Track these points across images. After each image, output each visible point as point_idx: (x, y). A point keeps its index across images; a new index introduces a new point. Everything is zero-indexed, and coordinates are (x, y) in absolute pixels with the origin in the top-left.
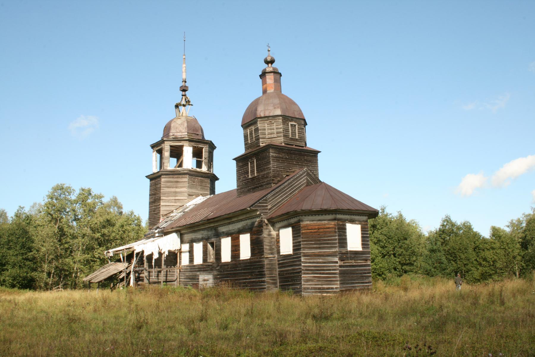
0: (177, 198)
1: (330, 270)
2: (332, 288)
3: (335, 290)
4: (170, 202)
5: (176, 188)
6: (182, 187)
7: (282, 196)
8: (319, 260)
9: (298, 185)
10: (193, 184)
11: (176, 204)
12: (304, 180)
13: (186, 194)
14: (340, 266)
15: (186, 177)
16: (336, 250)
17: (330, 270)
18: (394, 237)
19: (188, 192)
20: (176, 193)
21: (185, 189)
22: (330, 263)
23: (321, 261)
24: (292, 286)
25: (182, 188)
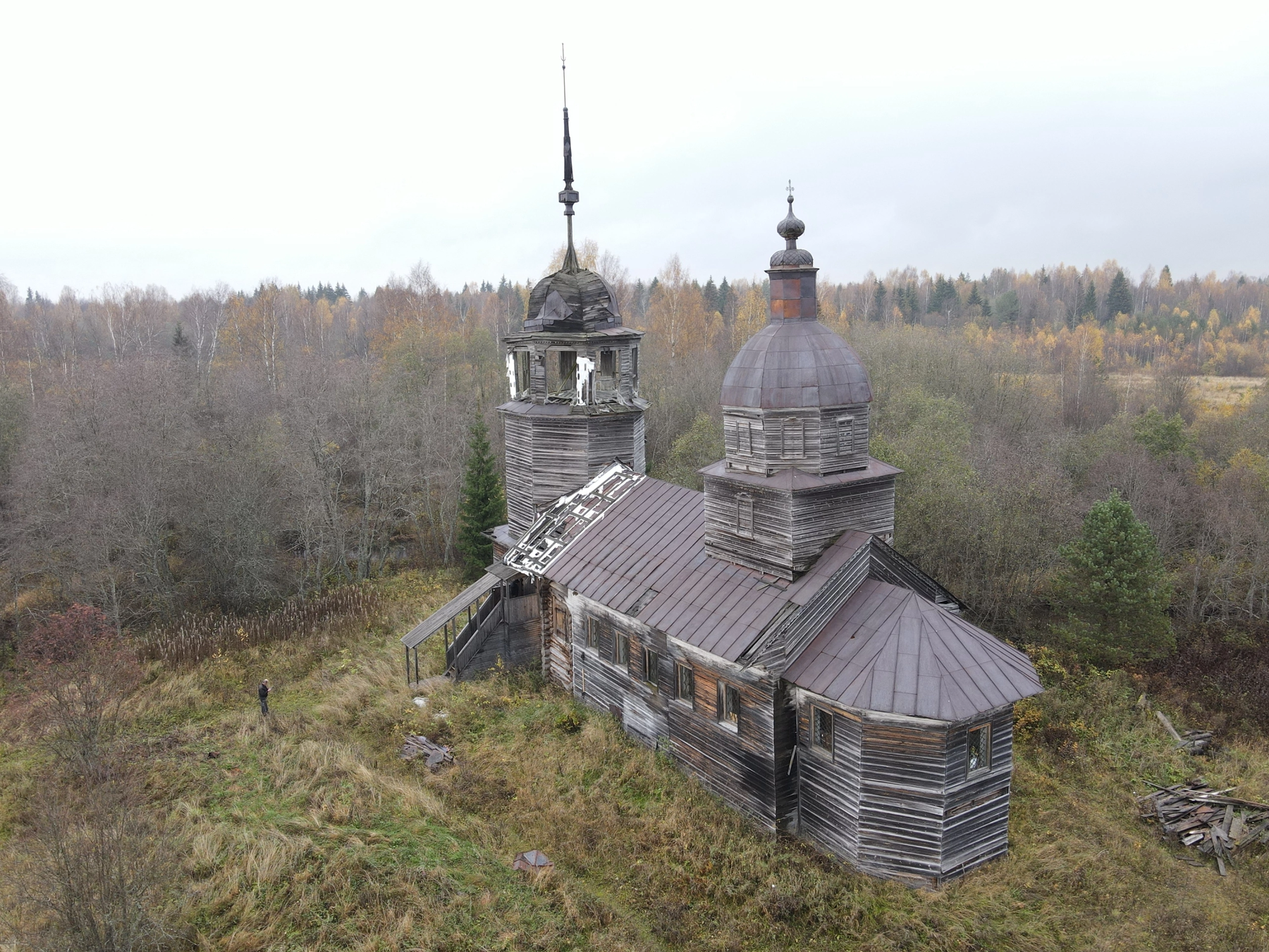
0: (566, 471)
1: (923, 829)
2: (925, 867)
3: (930, 871)
4: (552, 478)
5: (565, 449)
6: (577, 448)
7: (820, 612)
8: (898, 805)
9: (851, 579)
10: (599, 440)
11: (564, 484)
12: (864, 566)
13: (585, 464)
14: (862, 803)
15: (585, 428)
16: (939, 793)
17: (923, 829)
18: (518, 752)
19: (590, 459)
20: (564, 459)
21: (583, 452)
22: (924, 816)
23: (903, 806)
24: (465, 631)
25: (576, 450)
